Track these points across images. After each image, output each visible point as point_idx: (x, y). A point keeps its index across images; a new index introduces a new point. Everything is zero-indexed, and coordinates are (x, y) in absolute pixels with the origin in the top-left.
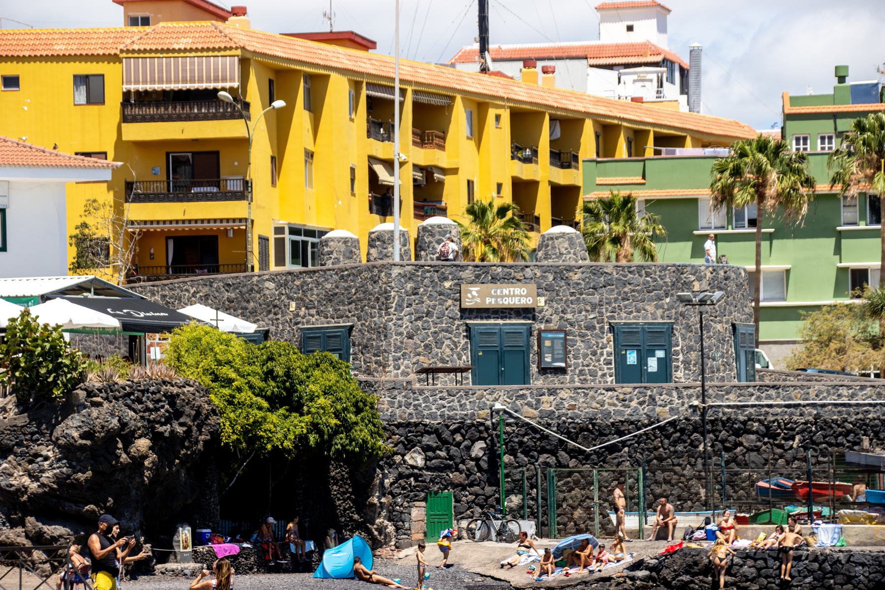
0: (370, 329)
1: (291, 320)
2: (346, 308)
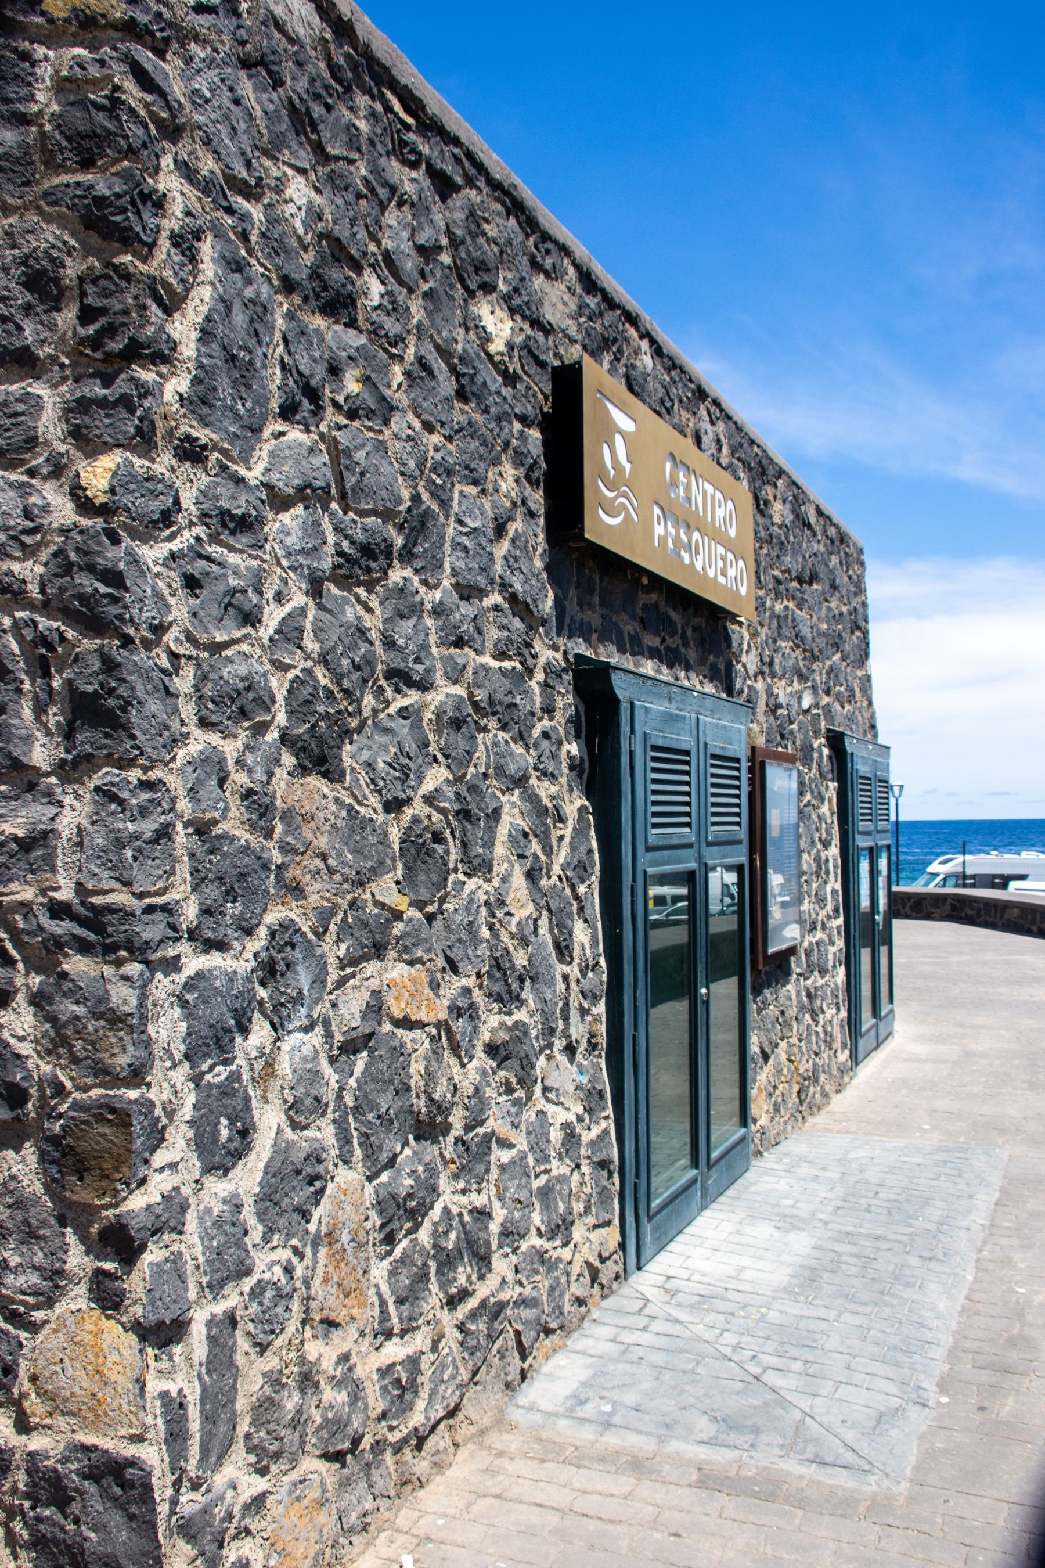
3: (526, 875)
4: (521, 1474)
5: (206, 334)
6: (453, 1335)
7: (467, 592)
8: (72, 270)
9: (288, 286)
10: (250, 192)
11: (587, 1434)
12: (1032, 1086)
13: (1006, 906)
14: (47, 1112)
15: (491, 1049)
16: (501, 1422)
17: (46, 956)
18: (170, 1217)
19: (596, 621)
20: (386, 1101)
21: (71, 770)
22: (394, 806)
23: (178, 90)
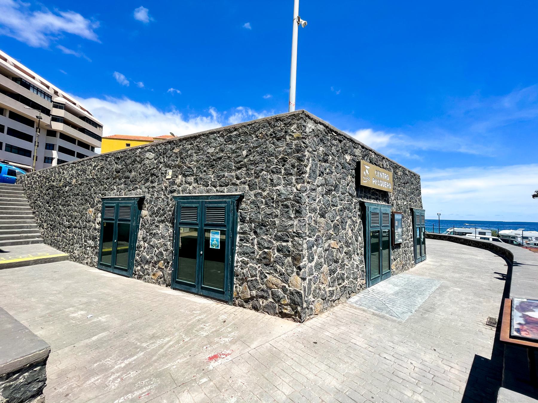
0: (270, 201)
1: (166, 188)
2: (233, 174)
3: (352, 230)
4: (347, 308)
5: (310, 169)
6: (339, 289)
7: (343, 194)
8: (296, 164)
9: (320, 161)
10: (315, 151)
11: (357, 306)
12: (453, 272)
13: (497, 247)
14: (292, 253)
15: (345, 253)
16: (345, 302)
17: (293, 237)
18: (305, 267)
19: (363, 195)
20: (330, 257)
21: (295, 218)
22: (332, 221)
23: (307, 143)
